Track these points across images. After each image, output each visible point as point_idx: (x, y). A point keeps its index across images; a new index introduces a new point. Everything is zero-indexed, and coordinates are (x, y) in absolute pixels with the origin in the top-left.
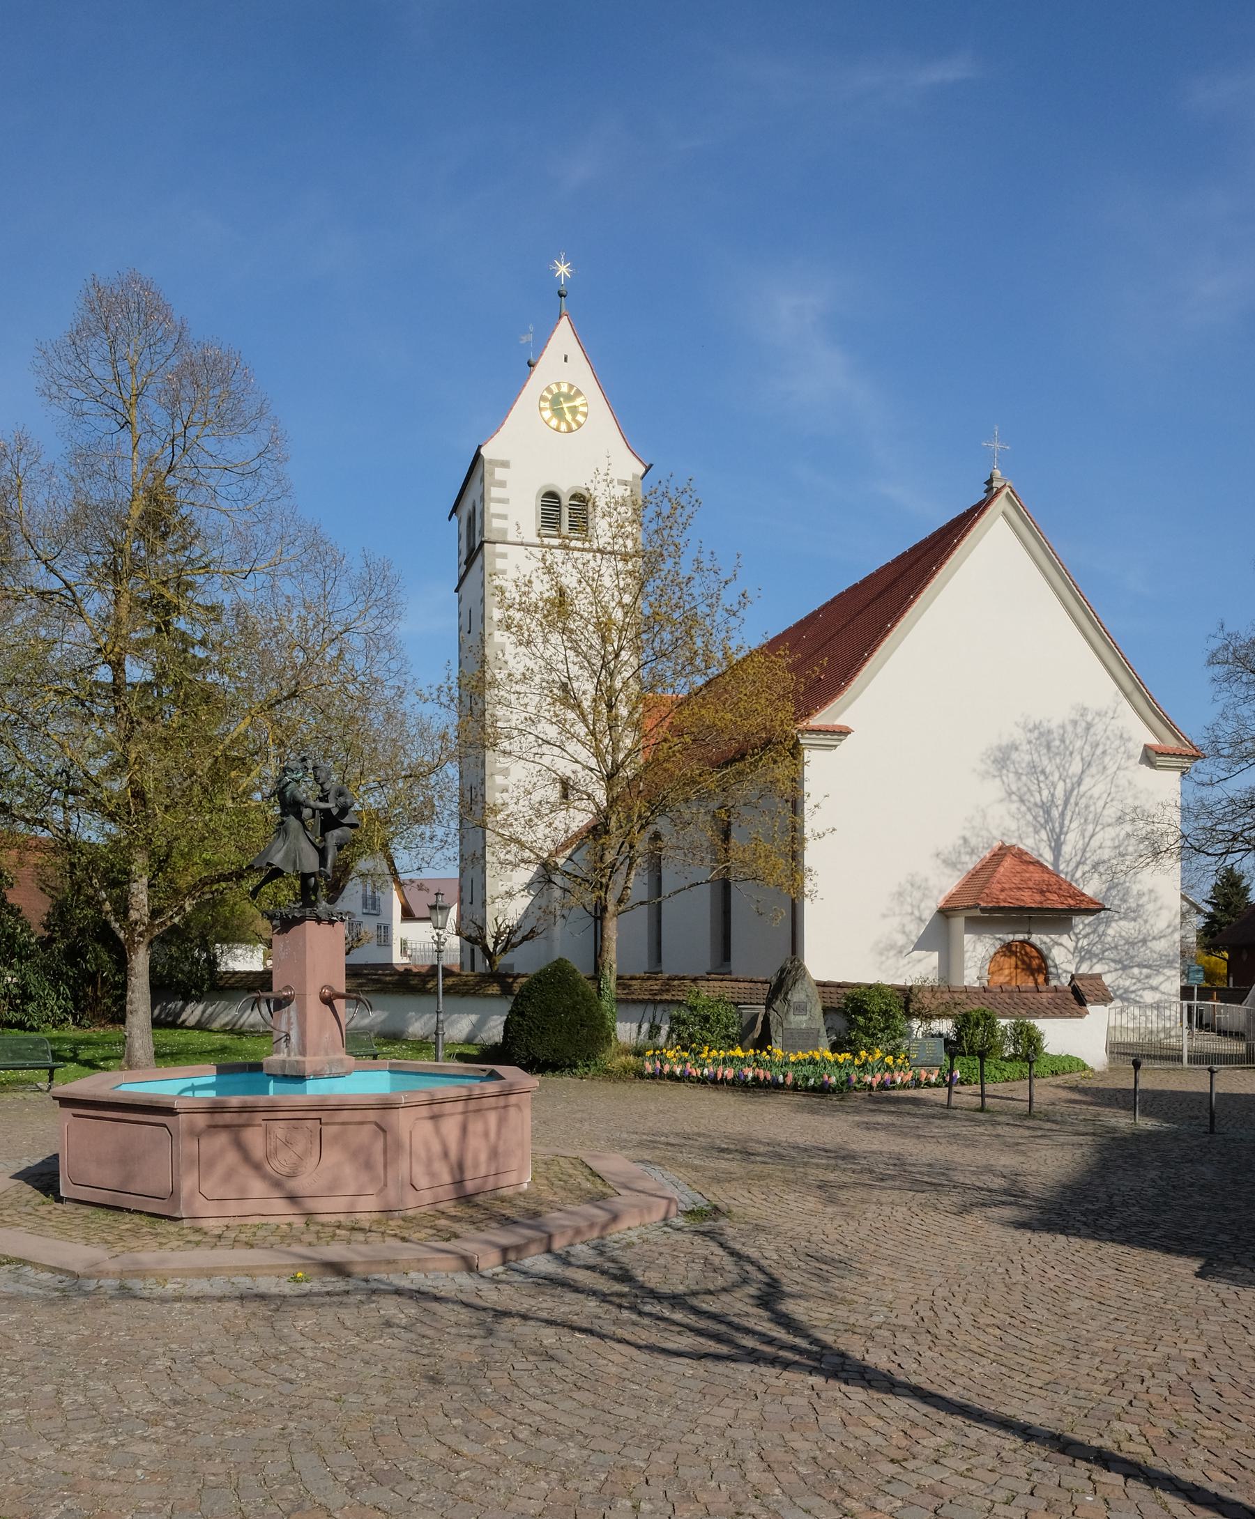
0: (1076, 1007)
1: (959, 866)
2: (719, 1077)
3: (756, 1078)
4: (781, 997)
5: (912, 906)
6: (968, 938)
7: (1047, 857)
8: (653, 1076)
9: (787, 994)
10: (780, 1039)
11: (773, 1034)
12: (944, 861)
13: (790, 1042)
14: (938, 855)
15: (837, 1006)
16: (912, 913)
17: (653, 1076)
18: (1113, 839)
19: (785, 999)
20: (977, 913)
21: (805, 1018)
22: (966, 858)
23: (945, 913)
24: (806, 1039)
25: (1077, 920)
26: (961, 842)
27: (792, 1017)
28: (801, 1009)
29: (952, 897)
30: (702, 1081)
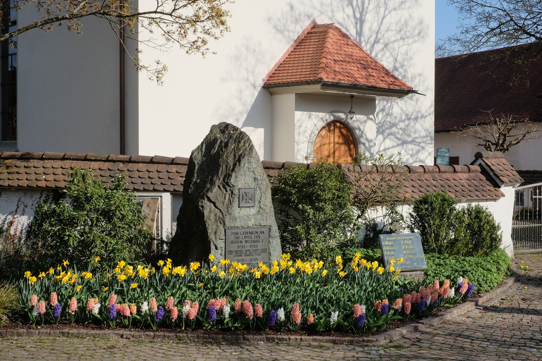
0: (492, 188)
1: (286, 33)
2: (175, 315)
3: (238, 315)
4: (218, 182)
5: (248, 71)
6: (298, 114)
7: (352, 32)
8: (47, 320)
9: (228, 176)
10: (221, 244)
11: (212, 237)
12: (275, 27)
13: (234, 247)
14: (269, 19)
15: (43, 184)
16: (247, 79)
17: (47, 320)
18: (397, 24)
19: (226, 184)
20: (317, 88)
21: (253, 211)
22: (291, 27)
23: (271, 88)
24: (247, 243)
25: (380, 103)
26: (288, 8)
27: (236, 211)
28: (246, 198)
29: (281, 67)
30: (141, 323)
